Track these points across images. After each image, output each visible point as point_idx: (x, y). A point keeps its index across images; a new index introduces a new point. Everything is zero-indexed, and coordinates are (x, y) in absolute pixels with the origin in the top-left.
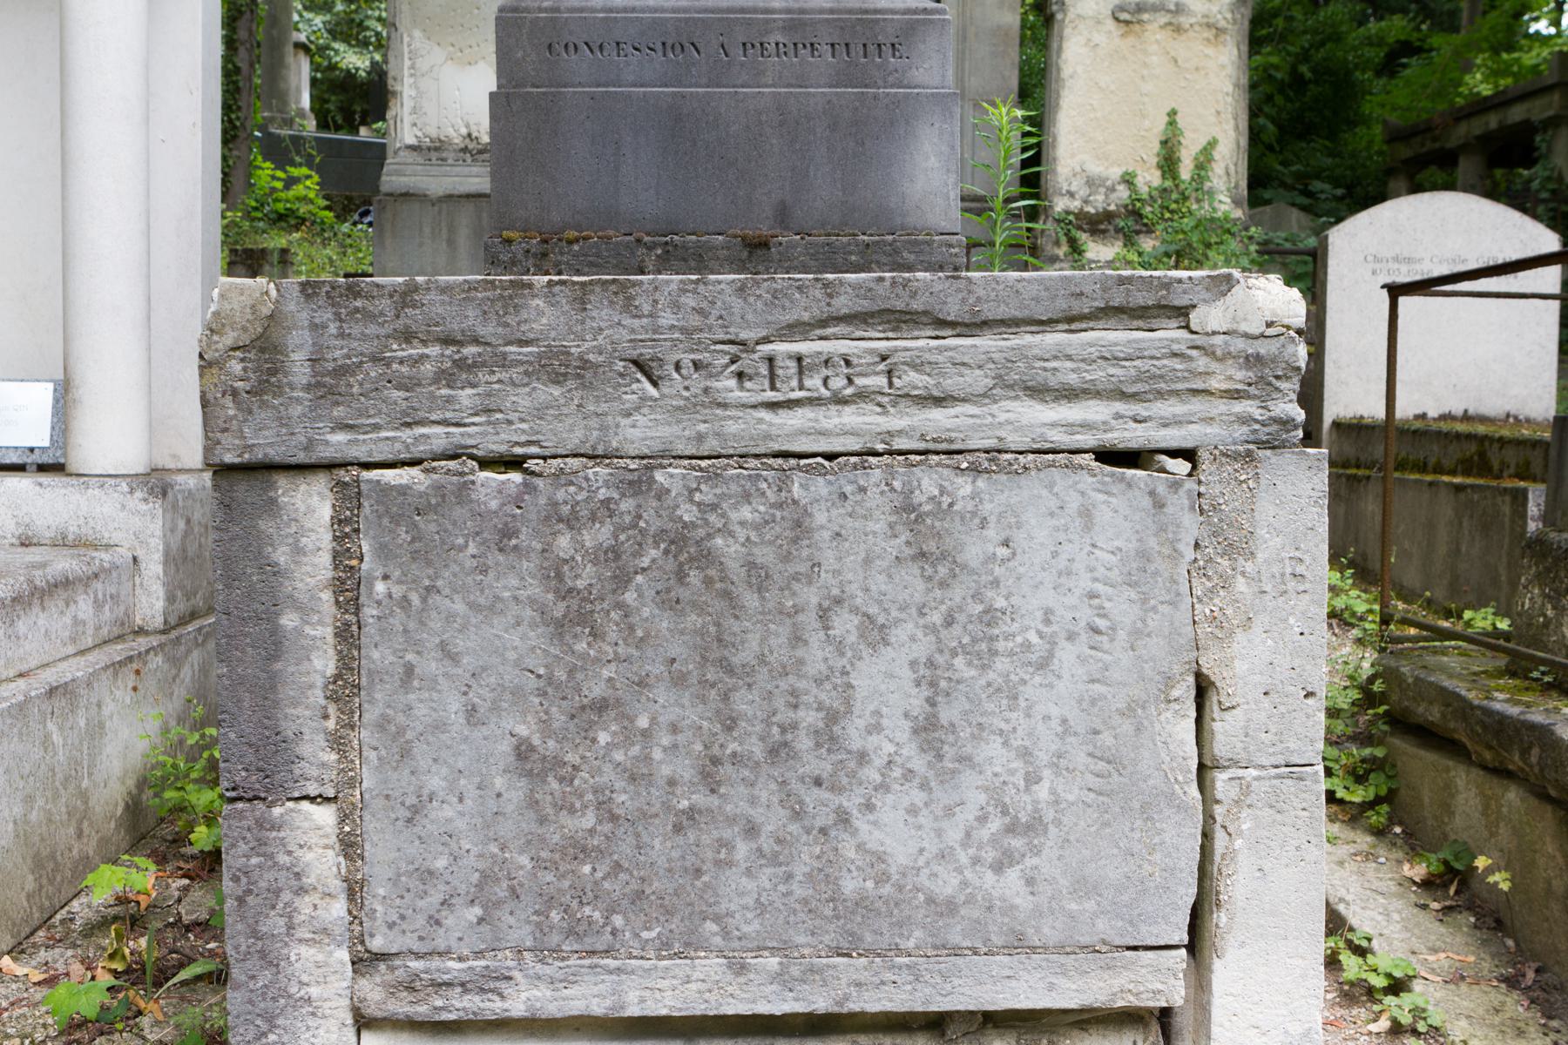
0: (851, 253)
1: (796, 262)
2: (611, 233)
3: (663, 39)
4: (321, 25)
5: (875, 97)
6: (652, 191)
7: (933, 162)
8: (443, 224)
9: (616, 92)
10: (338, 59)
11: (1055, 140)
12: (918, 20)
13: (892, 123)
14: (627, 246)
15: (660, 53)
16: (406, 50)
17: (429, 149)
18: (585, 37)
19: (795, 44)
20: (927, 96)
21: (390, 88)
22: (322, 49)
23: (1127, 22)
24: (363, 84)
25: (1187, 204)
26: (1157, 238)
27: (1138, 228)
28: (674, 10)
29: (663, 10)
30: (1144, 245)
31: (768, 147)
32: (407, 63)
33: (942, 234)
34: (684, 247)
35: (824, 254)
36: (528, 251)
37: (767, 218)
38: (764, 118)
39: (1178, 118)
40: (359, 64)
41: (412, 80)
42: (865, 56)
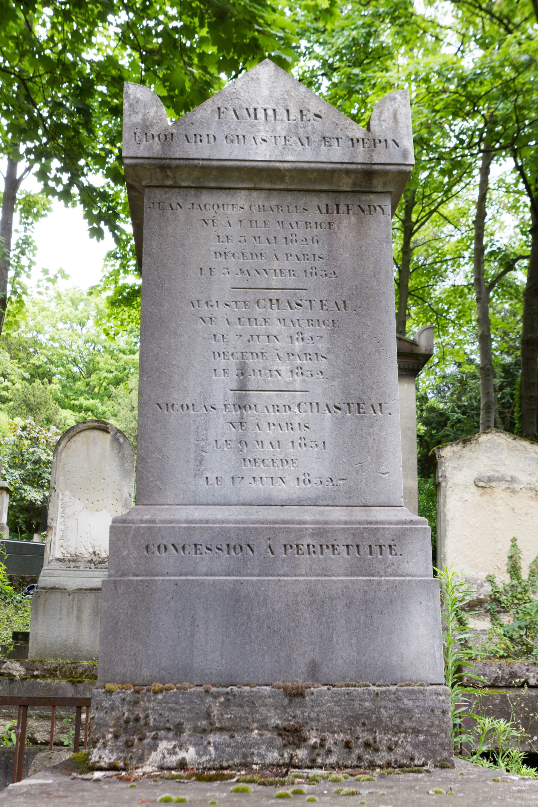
0: (365, 700)
1: (324, 708)
2: (187, 684)
3: (228, 542)
4: (18, 476)
5: (379, 583)
6: (218, 653)
7: (422, 630)
8: (75, 606)
9: (193, 580)
10: (26, 495)
11: (445, 556)
12: (407, 529)
13: (391, 602)
14: (198, 695)
15: (226, 552)
16: (60, 502)
17: (69, 561)
18: (173, 541)
19: (321, 546)
20: (415, 582)
21: (48, 524)
22: (17, 489)
23: (483, 487)
24: (38, 508)
25: (527, 595)
26: (510, 616)
27: (499, 609)
28: (236, 522)
29: (228, 522)
30: (503, 620)
31: (303, 619)
32: (60, 510)
33: (431, 684)
34: (241, 696)
35: (345, 701)
36: (124, 700)
37: (302, 673)
38: (299, 599)
39: (517, 543)
40: (37, 497)
41: (62, 520)
42: (371, 554)
